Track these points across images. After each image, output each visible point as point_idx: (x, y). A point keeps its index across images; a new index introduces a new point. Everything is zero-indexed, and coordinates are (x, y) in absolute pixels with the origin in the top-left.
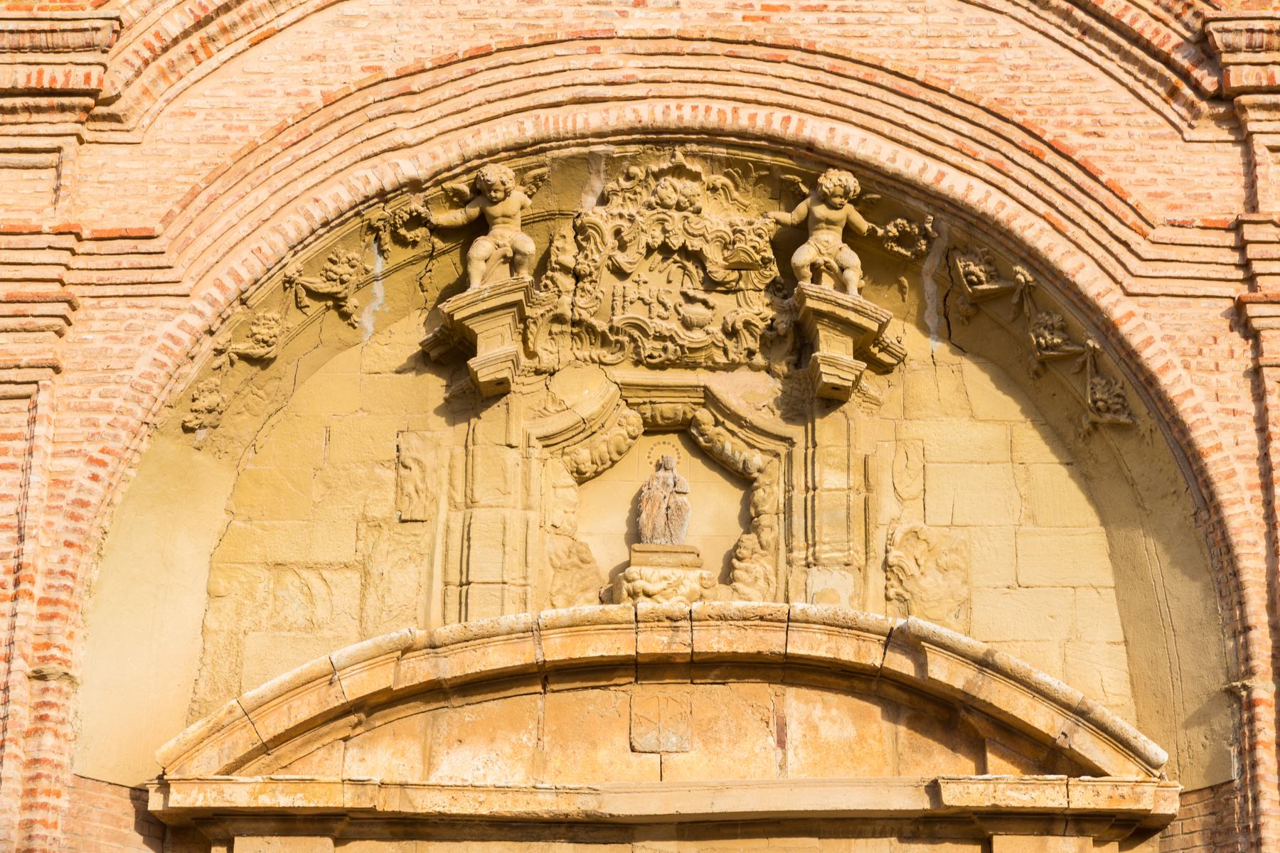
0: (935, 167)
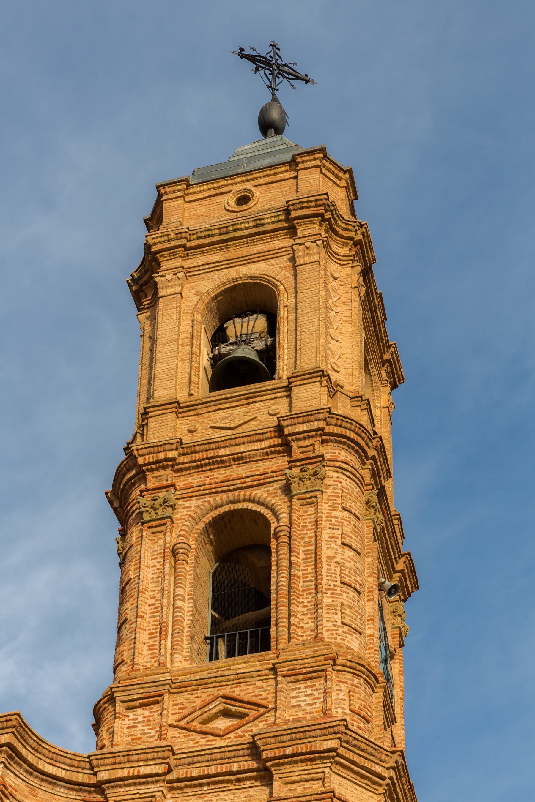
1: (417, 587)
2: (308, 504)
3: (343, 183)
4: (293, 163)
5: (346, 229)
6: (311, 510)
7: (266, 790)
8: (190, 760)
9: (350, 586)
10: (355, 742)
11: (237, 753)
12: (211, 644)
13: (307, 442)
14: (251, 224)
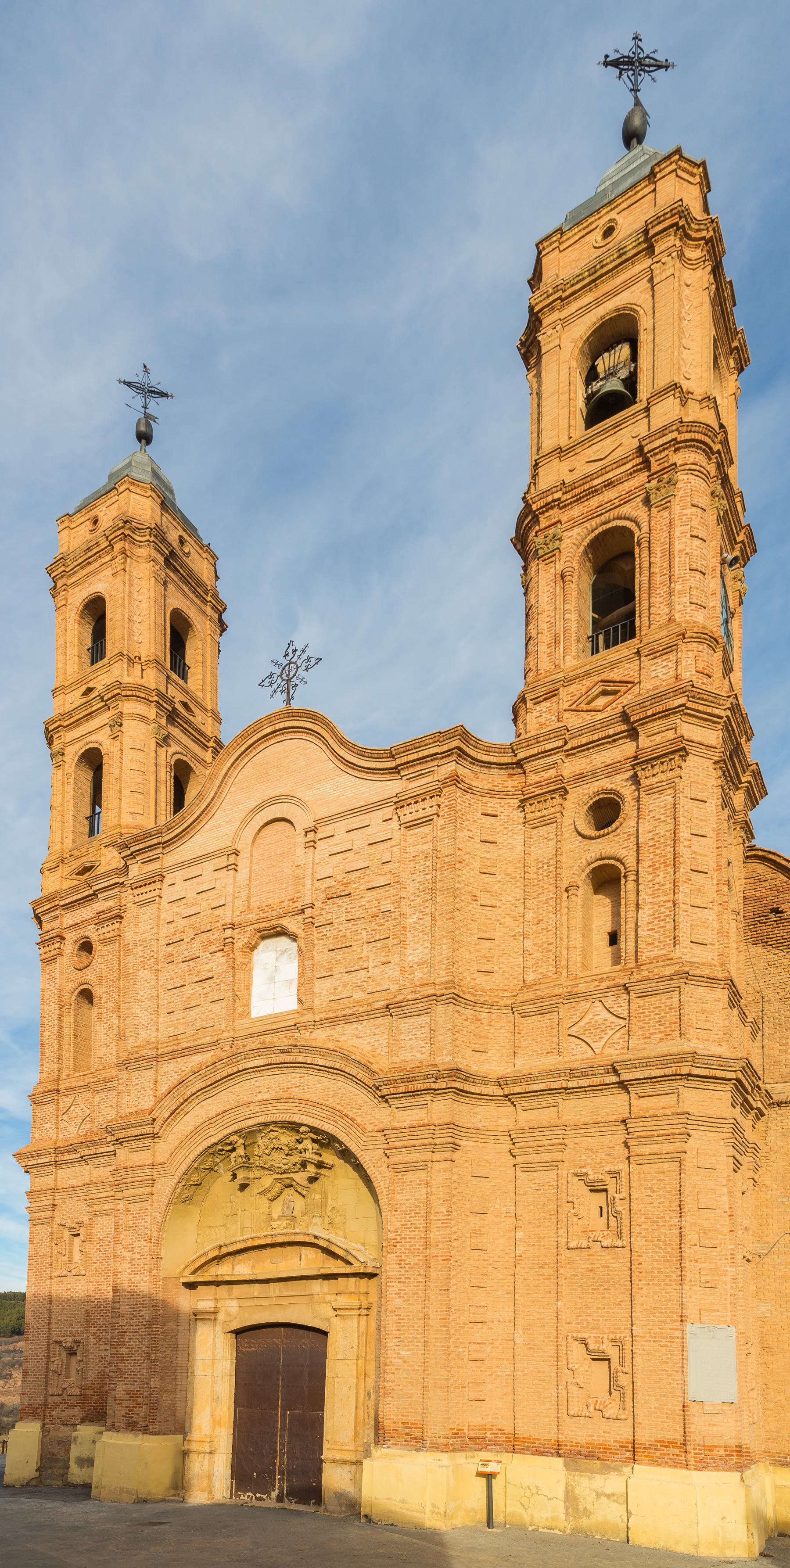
0: (322, 1123)
1: (755, 551)
2: (664, 509)
3: (697, 179)
4: (652, 177)
5: (698, 230)
6: (666, 514)
7: (634, 744)
8: (580, 733)
9: (697, 570)
10: (700, 696)
11: (612, 721)
12: (593, 641)
13: (663, 455)
14: (615, 256)
